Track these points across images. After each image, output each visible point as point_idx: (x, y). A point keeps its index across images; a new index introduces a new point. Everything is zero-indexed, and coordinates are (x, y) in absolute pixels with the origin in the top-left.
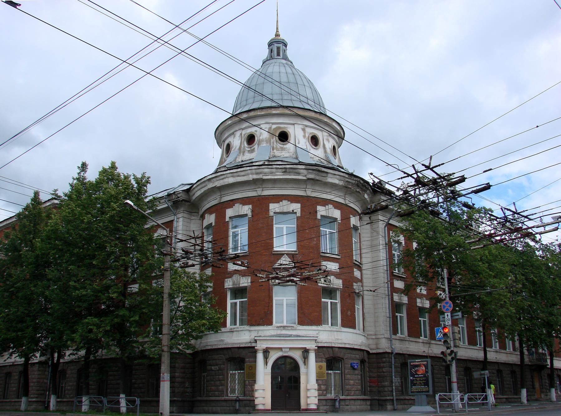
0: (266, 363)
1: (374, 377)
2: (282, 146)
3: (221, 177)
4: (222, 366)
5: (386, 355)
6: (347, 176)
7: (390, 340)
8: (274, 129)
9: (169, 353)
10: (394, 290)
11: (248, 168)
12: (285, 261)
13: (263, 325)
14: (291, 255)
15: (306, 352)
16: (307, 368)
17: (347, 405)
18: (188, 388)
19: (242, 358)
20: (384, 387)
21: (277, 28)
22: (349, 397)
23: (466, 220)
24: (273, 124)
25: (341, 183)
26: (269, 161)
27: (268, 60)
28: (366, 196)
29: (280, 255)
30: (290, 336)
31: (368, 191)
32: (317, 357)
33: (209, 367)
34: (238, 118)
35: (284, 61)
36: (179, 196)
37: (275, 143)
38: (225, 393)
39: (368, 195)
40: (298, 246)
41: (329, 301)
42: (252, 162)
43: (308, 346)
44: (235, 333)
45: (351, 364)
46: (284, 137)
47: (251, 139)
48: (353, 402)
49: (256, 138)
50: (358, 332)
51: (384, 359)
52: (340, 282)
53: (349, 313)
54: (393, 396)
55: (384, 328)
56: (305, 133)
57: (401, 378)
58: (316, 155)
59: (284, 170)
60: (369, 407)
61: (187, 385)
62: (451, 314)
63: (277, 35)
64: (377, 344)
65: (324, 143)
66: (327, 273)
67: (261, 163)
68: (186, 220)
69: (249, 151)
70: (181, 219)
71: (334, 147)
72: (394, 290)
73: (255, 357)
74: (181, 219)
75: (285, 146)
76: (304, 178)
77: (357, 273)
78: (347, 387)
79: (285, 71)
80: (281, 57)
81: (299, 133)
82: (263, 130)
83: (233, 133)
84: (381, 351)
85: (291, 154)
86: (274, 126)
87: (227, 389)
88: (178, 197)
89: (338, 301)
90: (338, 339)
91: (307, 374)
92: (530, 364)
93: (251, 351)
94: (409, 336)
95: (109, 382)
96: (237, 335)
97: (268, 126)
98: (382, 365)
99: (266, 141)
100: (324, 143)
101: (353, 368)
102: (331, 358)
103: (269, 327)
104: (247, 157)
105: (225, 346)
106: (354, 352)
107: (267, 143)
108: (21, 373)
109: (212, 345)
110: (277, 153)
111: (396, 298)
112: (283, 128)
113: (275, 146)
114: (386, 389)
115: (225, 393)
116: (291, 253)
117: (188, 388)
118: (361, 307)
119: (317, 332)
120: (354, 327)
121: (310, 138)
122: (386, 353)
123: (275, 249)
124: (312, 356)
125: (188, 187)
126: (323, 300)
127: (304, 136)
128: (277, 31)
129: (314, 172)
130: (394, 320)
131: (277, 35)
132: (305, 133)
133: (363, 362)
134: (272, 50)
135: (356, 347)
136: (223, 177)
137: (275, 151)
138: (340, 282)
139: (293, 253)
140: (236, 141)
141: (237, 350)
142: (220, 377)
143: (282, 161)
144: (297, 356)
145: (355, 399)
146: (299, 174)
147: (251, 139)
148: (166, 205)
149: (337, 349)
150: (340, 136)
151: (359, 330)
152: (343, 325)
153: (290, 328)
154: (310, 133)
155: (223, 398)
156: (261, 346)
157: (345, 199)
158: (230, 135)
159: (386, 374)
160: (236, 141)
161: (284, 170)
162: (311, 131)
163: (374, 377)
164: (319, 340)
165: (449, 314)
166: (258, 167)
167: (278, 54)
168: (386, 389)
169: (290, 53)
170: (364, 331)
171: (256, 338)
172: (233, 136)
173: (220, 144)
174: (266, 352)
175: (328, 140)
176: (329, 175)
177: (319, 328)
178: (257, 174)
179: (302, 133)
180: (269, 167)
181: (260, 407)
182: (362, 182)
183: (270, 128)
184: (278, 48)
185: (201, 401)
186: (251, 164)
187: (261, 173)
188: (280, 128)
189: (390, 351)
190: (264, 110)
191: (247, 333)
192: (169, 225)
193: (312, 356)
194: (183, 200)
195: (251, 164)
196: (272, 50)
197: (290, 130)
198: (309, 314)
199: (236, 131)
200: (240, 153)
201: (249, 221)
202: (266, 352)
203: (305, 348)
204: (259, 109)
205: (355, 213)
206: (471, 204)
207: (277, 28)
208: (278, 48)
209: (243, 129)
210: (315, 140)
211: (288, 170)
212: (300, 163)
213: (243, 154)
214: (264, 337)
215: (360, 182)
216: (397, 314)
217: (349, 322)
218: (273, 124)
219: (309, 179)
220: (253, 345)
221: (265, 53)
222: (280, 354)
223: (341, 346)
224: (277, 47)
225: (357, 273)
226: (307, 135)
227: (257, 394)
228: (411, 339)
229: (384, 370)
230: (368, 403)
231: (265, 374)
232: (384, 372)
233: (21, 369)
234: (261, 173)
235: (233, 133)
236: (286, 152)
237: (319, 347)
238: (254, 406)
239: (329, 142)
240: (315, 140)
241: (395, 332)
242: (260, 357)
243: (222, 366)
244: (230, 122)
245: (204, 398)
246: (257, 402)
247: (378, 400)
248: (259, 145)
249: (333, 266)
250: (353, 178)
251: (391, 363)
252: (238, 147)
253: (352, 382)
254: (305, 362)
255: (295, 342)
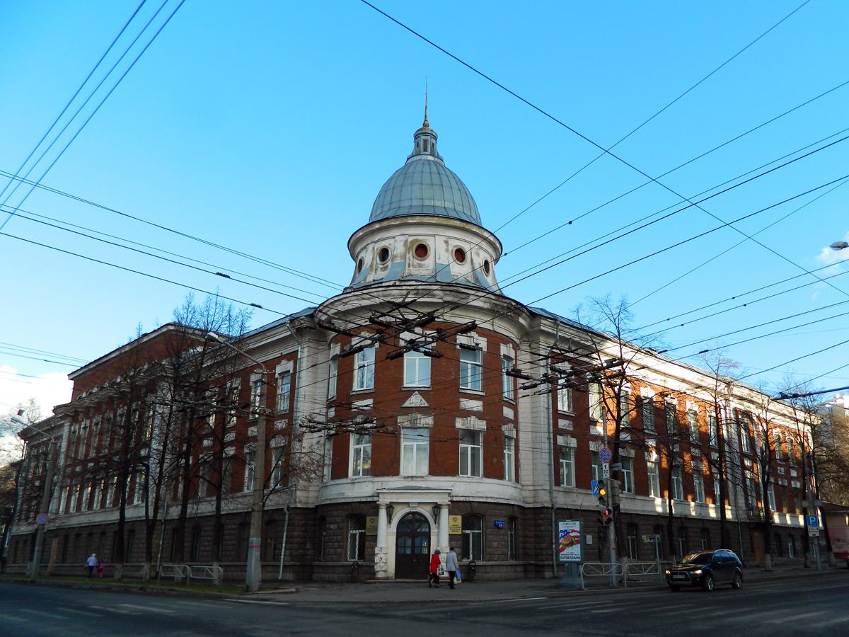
0: (390, 521)
1: (531, 537)
2: (419, 262)
3: (345, 301)
4: (341, 525)
5: (545, 511)
6: (493, 297)
7: (551, 492)
8: (411, 242)
9: (261, 513)
10: (558, 432)
11: (374, 290)
12: (416, 401)
13: (388, 475)
14: (423, 393)
15: (437, 508)
16: (439, 527)
17: (488, 572)
18: (309, 549)
19: (361, 514)
20: (542, 549)
21: (426, 116)
22: (490, 563)
23: (191, 391)
24: (410, 235)
25: (486, 306)
26: (400, 281)
27: (413, 156)
28: (521, 320)
29: (410, 392)
30: (420, 488)
31: (524, 315)
32: (450, 513)
33: (327, 526)
34: (379, 224)
35: (430, 158)
36: (302, 322)
37: (412, 259)
38: (343, 556)
39: (524, 319)
40: (432, 381)
41: (469, 447)
42: (381, 283)
43: (439, 501)
44: (356, 485)
45: (495, 522)
46: (422, 250)
47: (384, 254)
48: (496, 569)
49: (390, 253)
50: (509, 483)
51: (542, 516)
52: (484, 423)
53: (495, 460)
54: (552, 560)
55: (545, 479)
56: (448, 246)
57: (262, 539)
58: (460, 271)
59: (415, 292)
60: (522, 575)
61: (308, 546)
62: (610, 465)
63: (425, 125)
64: (535, 497)
65: (472, 258)
66: (467, 414)
67: (391, 283)
68: (312, 350)
69: (382, 268)
70: (306, 349)
71: (486, 263)
72: (558, 432)
73: (377, 514)
74: (306, 349)
75: (423, 262)
76: (440, 301)
77: (508, 412)
78: (488, 550)
79: (428, 170)
80: (429, 153)
81: (440, 245)
82: (397, 241)
83: (365, 247)
84: (539, 506)
85: (430, 272)
86: (411, 239)
87: (346, 553)
88: (301, 324)
89: (480, 447)
90: (478, 492)
91: (438, 534)
92: (748, 521)
93: (370, 507)
94: (577, 486)
95: (224, 542)
96: (357, 487)
97: (403, 238)
98: (540, 522)
99: (401, 256)
100: (472, 258)
101: (497, 527)
102: (471, 513)
103: (395, 478)
104: (381, 275)
105: (344, 501)
106: (499, 507)
107: (402, 259)
108: (115, 533)
109: (331, 499)
110: (413, 271)
111: (561, 440)
112: (421, 241)
113: (411, 263)
114: (544, 552)
115: (343, 556)
116: (423, 389)
117: (309, 549)
118: (513, 453)
119: (452, 483)
120: (501, 477)
121: (454, 252)
122: (544, 507)
123: (405, 385)
124: (444, 513)
125: (312, 311)
126: (461, 445)
127: (447, 250)
128: (426, 120)
129: (452, 293)
130: (558, 466)
131: (425, 125)
132: (448, 246)
133: (512, 519)
134: (418, 144)
135: (502, 501)
136: (347, 300)
137: (411, 268)
138: (484, 423)
139: (426, 389)
140: (369, 256)
141: (357, 505)
142: (339, 537)
143: (416, 280)
144: (426, 512)
145: (499, 566)
146: (434, 296)
147: (384, 254)
148: (289, 333)
149: (476, 504)
150: (497, 249)
151: (510, 480)
152: (487, 475)
153: (419, 479)
154: (455, 246)
155: (340, 563)
156: (384, 500)
157: (493, 325)
158: (362, 249)
159: (544, 533)
160: (369, 256)
161: (415, 292)
162: (454, 244)
163: (531, 537)
164: (452, 494)
165: (607, 465)
166: (385, 289)
167: (425, 150)
168: (544, 552)
169: (440, 148)
170: (517, 480)
171: (378, 491)
172: (365, 250)
173: (354, 257)
174: (390, 508)
175: (478, 254)
176: (472, 297)
177: (455, 479)
178: (384, 296)
179: (444, 245)
180: (399, 288)
181: (380, 575)
182: (514, 304)
183: (407, 241)
184: (426, 141)
185: (318, 566)
186: (380, 285)
187: (389, 295)
188: (417, 240)
189: (550, 506)
190: (399, 219)
191: (370, 485)
192: (293, 356)
193: (444, 513)
194: (307, 327)
195: (380, 285)
196: (418, 144)
197: (430, 242)
198: (443, 463)
199: (369, 244)
200: (372, 270)
201: (376, 352)
202: (390, 508)
203: (437, 503)
204: (394, 217)
205: (506, 340)
206: (474, 345)
207: (426, 116)
208: (426, 141)
209: (375, 242)
210: (460, 255)
211: (420, 291)
212: (437, 283)
213: (376, 272)
214: (388, 489)
215: (511, 304)
216: (561, 461)
217: (494, 470)
218: (410, 235)
219: (446, 302)
220: (376, 499)
221: (411, 148)
222: (407, 510)
223: (481, 500)
224: (424, 139)
225: (508, 412)
226: (450, 249)
227: (377, 559)
228: (580, 491)
229: (543, 528)
230: (519, 569)
231: (388, 534)
232: (542, 531)
233: (116, 528)
234: (389, 295)
235: (365, 247)
236: (426, 267)
237: (452, 501)
238: (374, 573)
239: (479, 256)
240: (460, 255)
241: (558, 482)
242: (383, 513)
243: (341, 525)
244: (361, 234)
245: (322, 563)
246: (377, 568)
247: (536, 565)
248: (392, 260)
249: (476, 405)
250: (501, 299)
251: (552, 520)
252: (369, 264)
253: (495, 544)
254: (435, 521)
255: (424, 496)
